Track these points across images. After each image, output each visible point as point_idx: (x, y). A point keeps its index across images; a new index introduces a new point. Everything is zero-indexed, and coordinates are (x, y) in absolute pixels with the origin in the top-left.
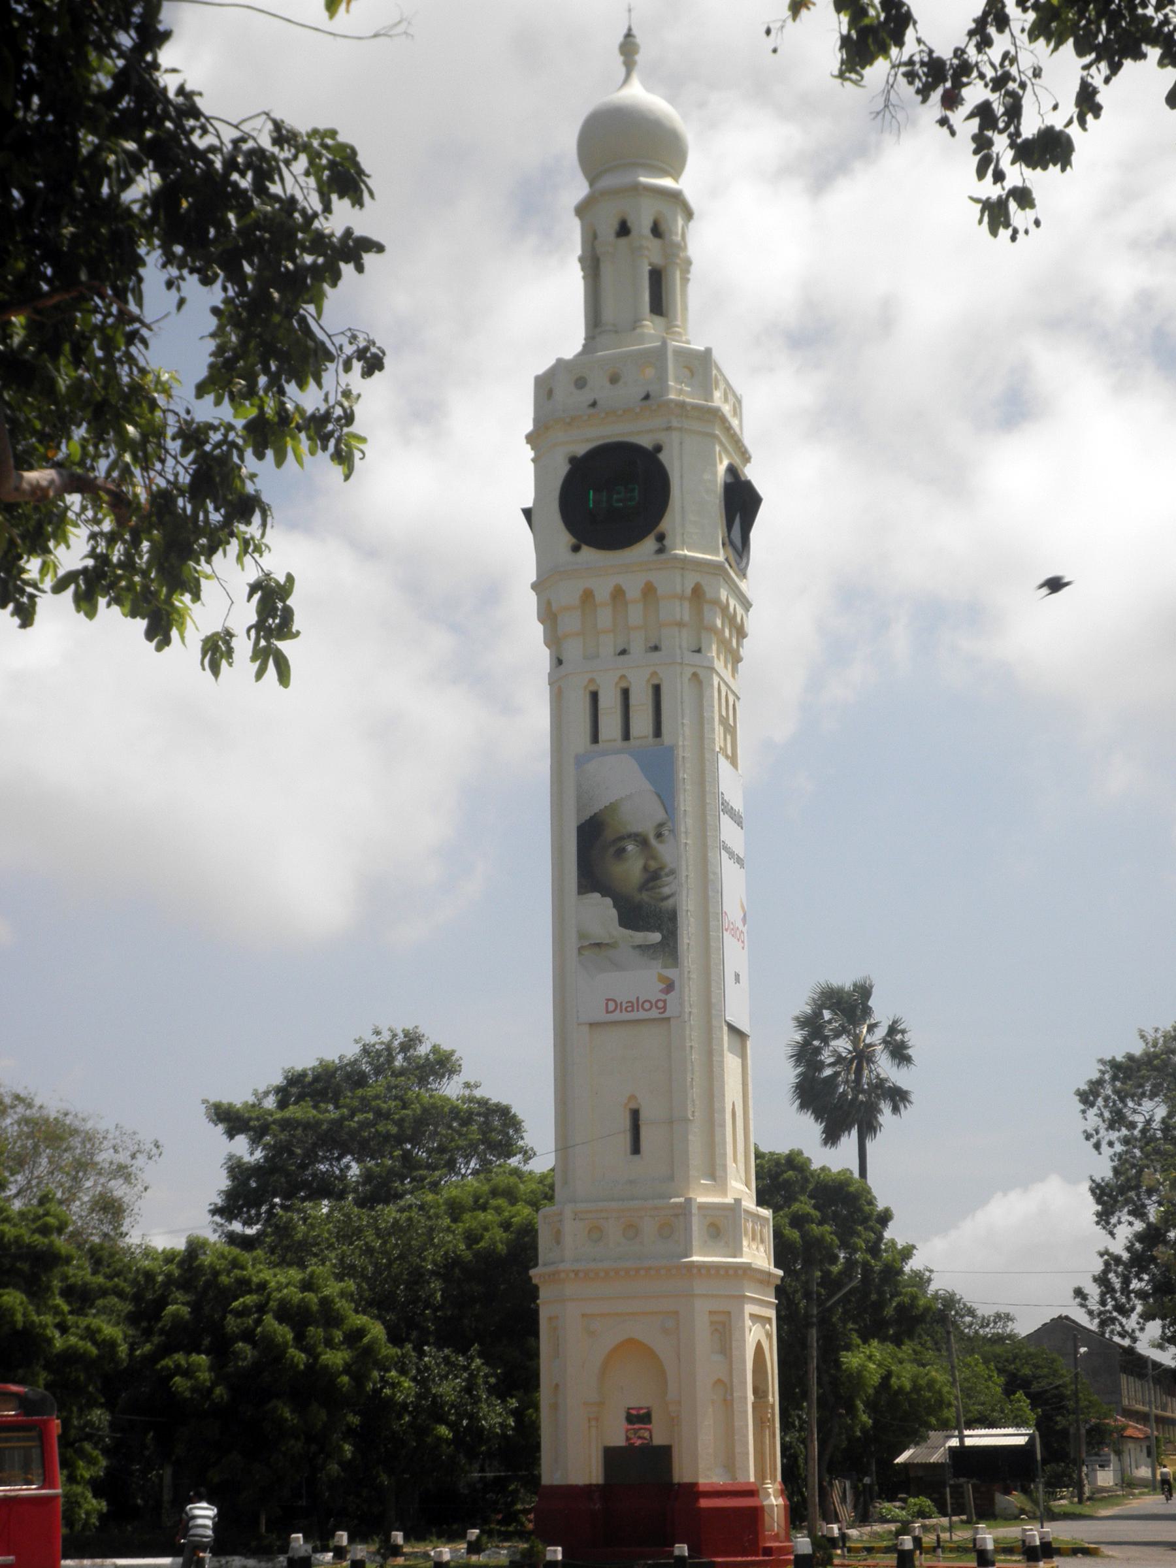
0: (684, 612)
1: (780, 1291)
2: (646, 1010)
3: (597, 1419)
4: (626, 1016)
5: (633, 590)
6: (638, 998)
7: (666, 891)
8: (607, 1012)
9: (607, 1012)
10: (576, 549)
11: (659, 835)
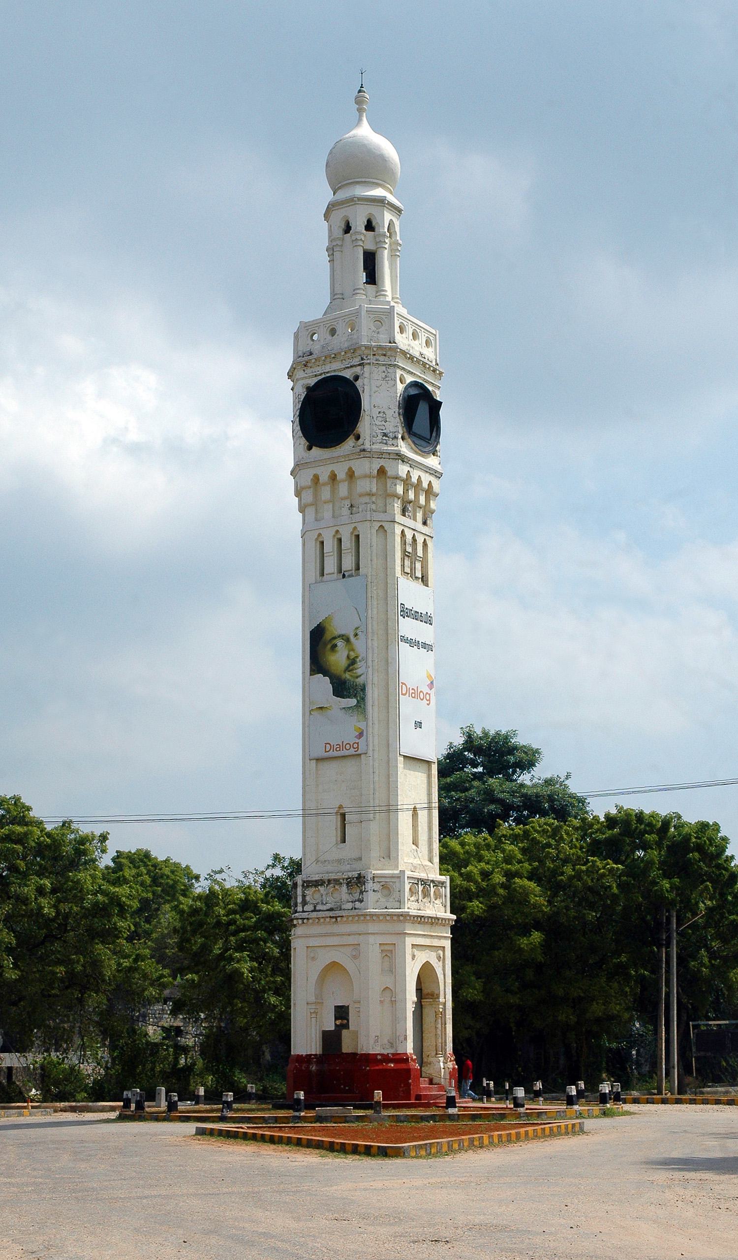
0: (373, 486)
1: (453, 929)
2: (347, 750)
3: (316, 1013)
4: (336, 754)
5: (341, 475)
6: (343, 742)
7: (359, 672)
8: (326, 752)
9: (326, 752)
10: (310, 448)
11: (356, 635)
